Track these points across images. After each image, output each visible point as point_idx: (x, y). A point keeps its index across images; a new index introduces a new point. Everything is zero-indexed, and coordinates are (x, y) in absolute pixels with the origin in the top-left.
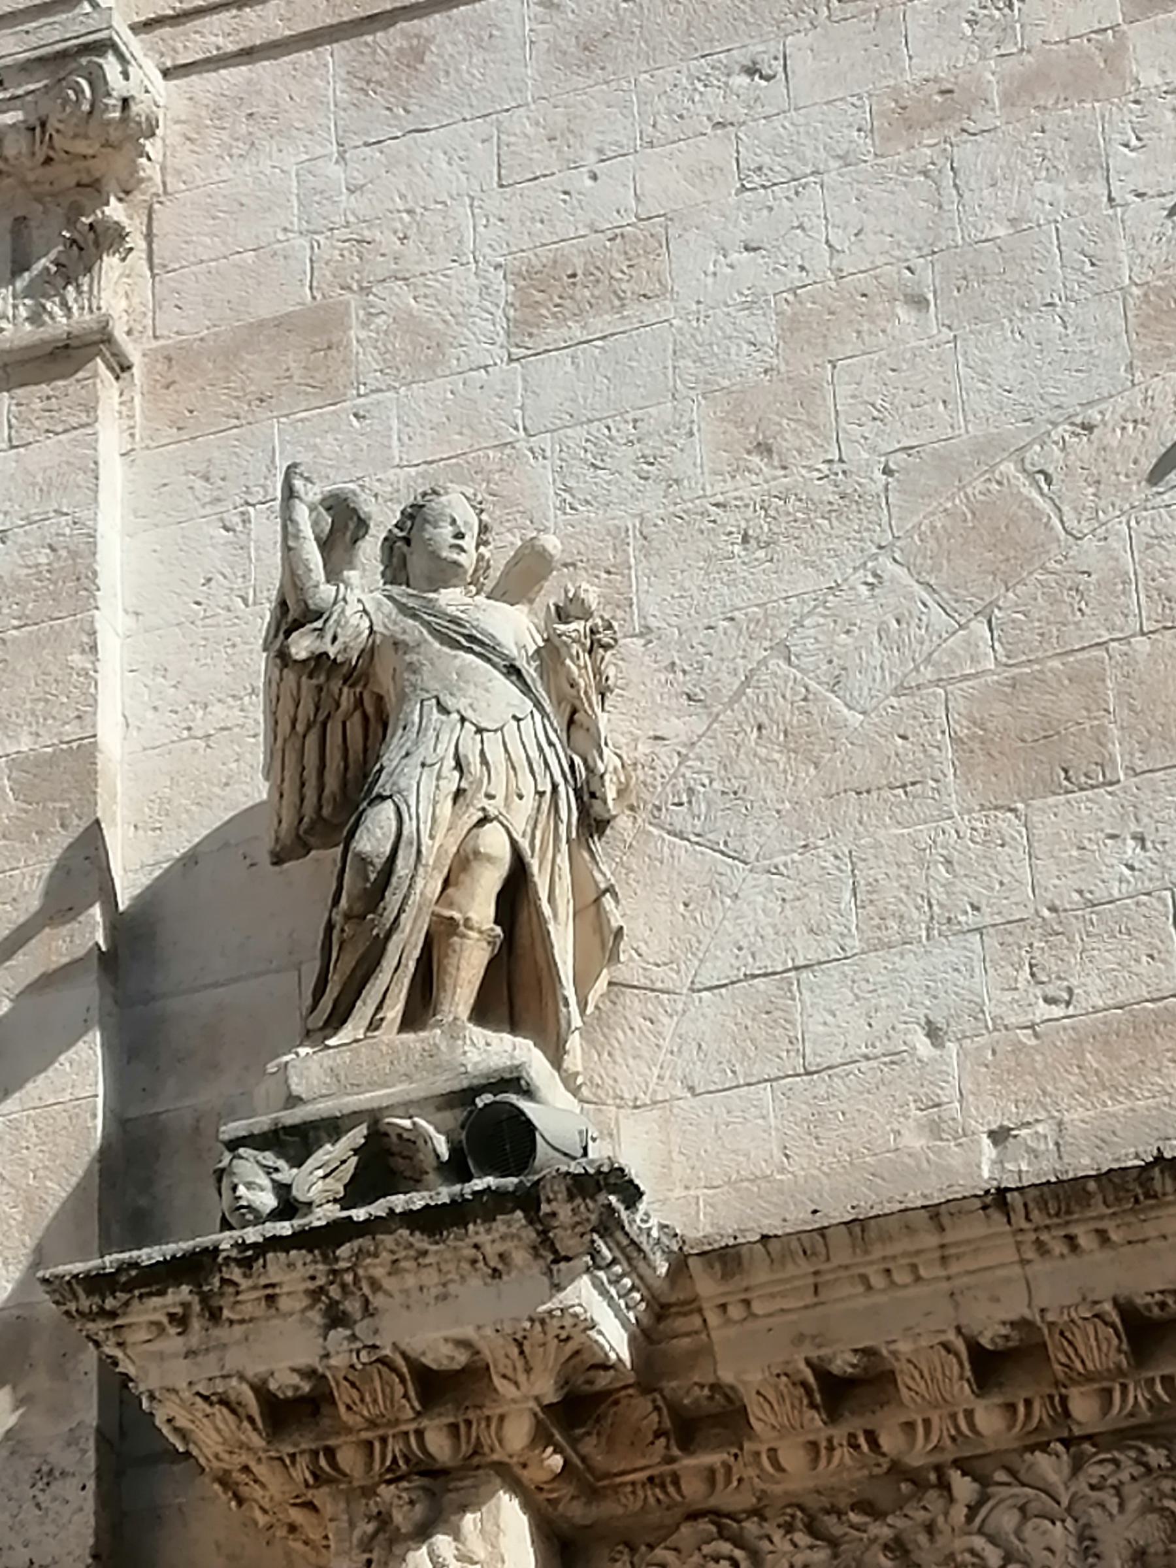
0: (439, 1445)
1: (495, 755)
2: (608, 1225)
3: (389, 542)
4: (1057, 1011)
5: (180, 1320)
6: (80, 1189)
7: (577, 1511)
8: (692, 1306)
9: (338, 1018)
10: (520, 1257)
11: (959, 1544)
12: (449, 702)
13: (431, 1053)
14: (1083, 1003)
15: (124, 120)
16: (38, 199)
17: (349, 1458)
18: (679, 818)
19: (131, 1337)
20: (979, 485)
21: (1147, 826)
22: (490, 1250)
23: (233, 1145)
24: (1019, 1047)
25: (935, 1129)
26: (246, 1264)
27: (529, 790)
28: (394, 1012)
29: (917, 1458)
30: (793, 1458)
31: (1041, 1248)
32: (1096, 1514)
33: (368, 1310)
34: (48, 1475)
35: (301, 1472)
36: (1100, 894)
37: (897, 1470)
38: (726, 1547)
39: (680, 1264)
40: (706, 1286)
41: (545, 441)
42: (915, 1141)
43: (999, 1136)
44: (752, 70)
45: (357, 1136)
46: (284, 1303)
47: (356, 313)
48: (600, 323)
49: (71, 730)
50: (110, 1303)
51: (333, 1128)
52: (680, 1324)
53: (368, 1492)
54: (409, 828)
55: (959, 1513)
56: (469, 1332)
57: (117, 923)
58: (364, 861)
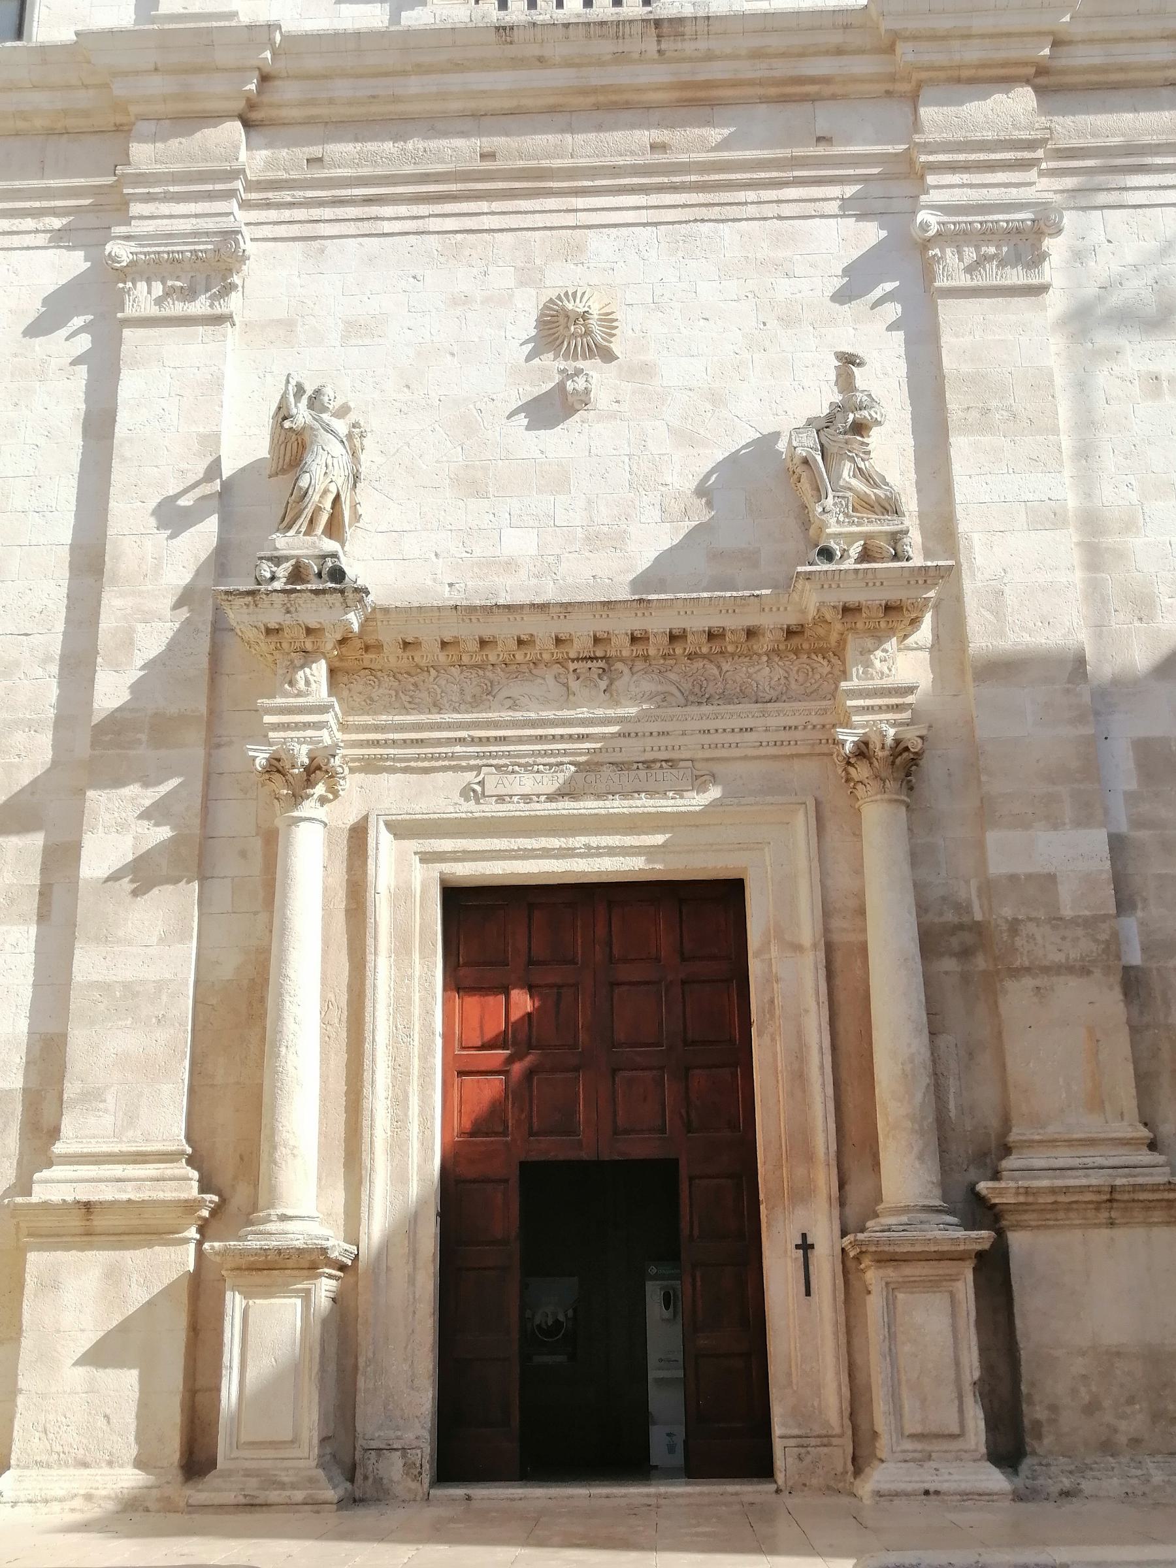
0: (309, 646)
1: (336, 464)
2: (361, 600)
3: (310, 398)
4: (469, 555)
5: (247, 605)
6: (209, 557)
7: (337, 664)
8: (374, 619)
9: (289, 527)
10: (337, 604)
11: (430, 686)
12: (325, 447)
13: (314, 543)
14: (474, 554)
15: (243, 255)
16: (214, 270)
17: (285, 645)
18: (376, 485)
19: (233, 607)
20: (463, 410)
21: (496, 511)
22: (330, 602)
23: (261, 558)
24: (458, 563)
25: (435, 580)
26: (267, 594)
27: (343, 475)
28: (303, 530)
29: (423, 663)
30: (393, 660)
31: (463, 620)
32: (465, 684)
33: (296, 611)
34: (197, 631)
35: (273, 646)
36: (482, 527)
37: (417, 665)
38: (372, 678)
39: (374, 609)
40: (379, 616)
41: (349, 372)
42: (429, 582)
43: (451, 585)
44: (414, 277)
45: (293, 562)
46: (275, 606)
47: (300, 323)
48: (367, 341)
49: (215, 428)
50: (230, 598)
51: (287, 558)
52: (371, 623)
53: (288, 654)
54: (313, 482)
55: (431, 679)
56: (322, 621)
57: (223, 484)
58: (301, 488)
